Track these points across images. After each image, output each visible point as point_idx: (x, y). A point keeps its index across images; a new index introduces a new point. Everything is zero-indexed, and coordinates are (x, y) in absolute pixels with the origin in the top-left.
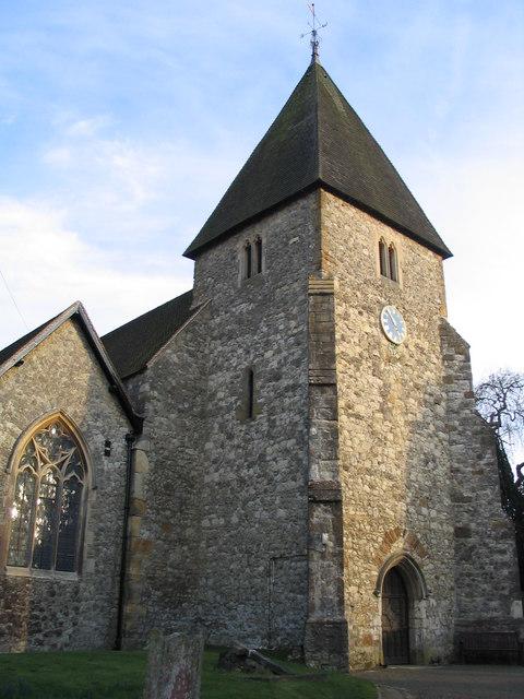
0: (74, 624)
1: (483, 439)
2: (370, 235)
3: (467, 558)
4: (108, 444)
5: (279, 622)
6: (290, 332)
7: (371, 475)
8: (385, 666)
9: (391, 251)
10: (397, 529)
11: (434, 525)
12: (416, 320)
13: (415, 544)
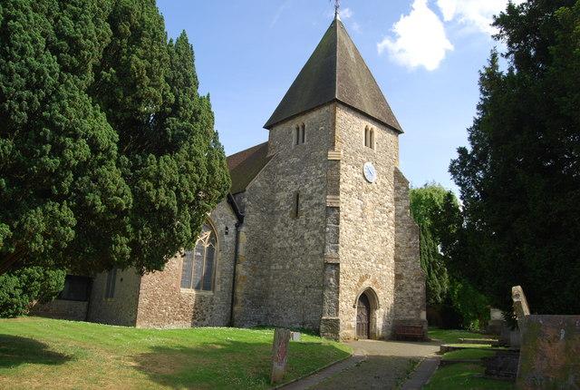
4: (227, 228)
9: (372, 132)
11: (385, 273)
13: (375, 282)
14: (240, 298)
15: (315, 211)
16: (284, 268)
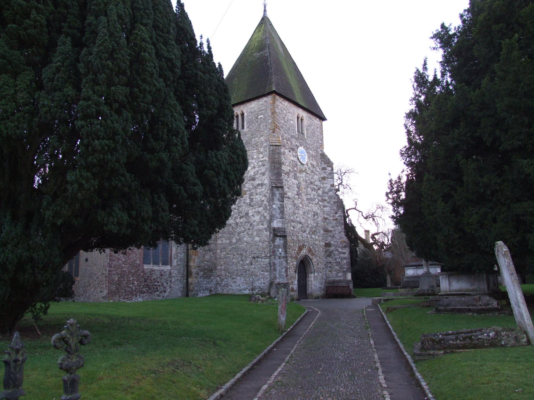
0: (170, 288)
1: (337, 205)
2: (293, 114)
3: (329, 255)
5: (257, 284)
6: (259, 160)
7: (293, 223)
8: (300, 300)
9: (302, 120)
10: (303, 245)
11: (317, 242)
12: (311, 152)
13: (310, 251)
14: (194, 271)
15: (258, 191)
16: (230, 243)
